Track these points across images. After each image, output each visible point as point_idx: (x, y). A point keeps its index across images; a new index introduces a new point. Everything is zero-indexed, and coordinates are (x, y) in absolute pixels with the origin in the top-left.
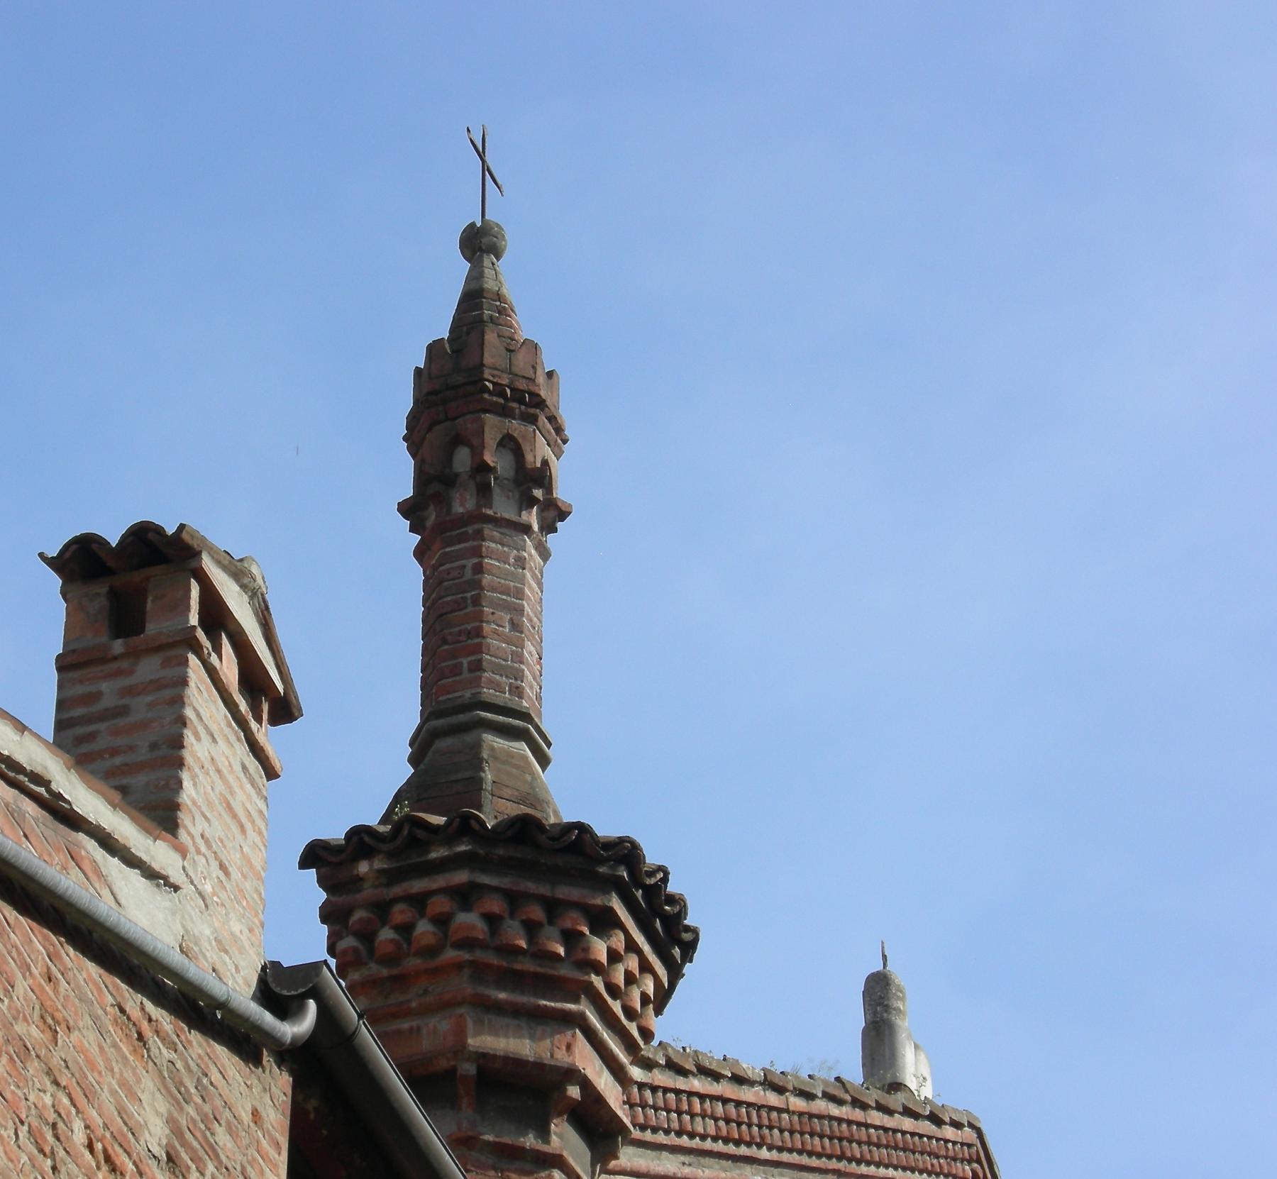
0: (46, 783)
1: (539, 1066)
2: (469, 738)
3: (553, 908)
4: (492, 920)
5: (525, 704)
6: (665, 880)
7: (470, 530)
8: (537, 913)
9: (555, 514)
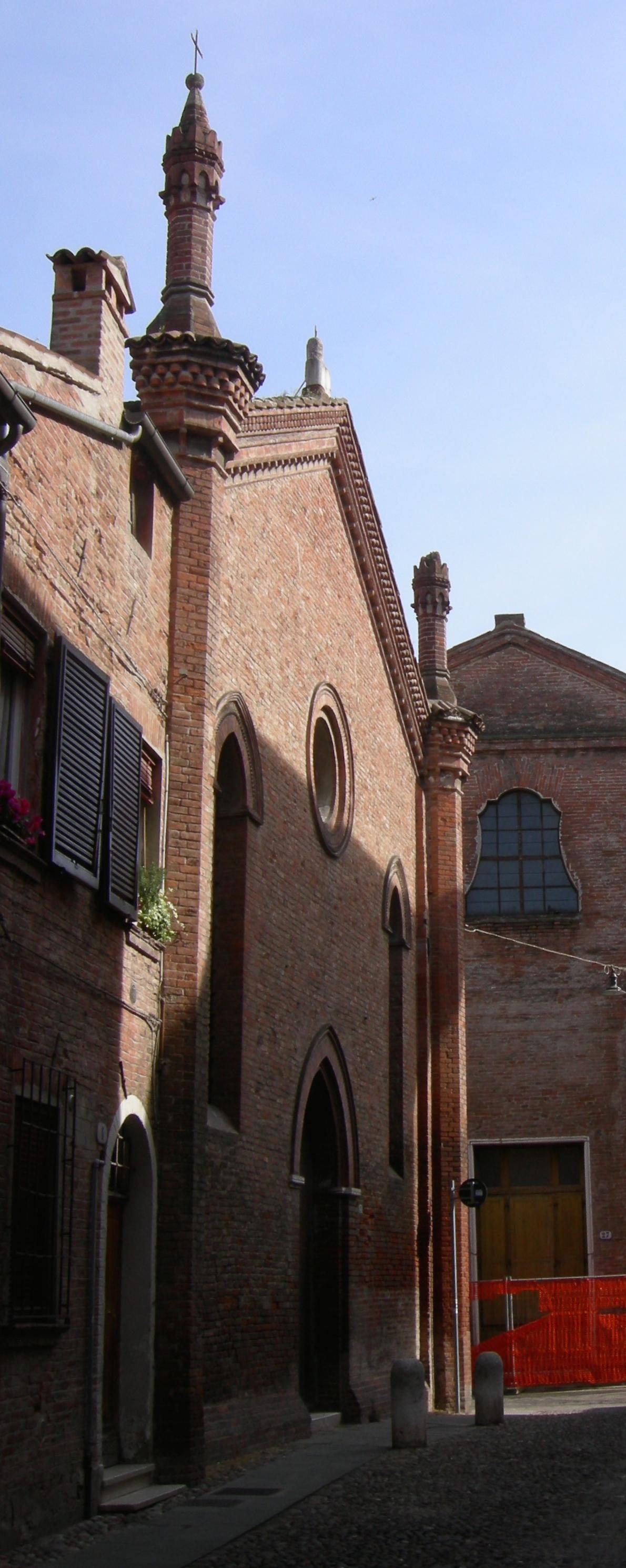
1: (209, 430)
2: (185, 296)
3: (216, 370)
4: (195, 375)
5: (206, 283)
6: (256, 360)
7: (187, 209)
8: (211, 373)
9: (219, 202)
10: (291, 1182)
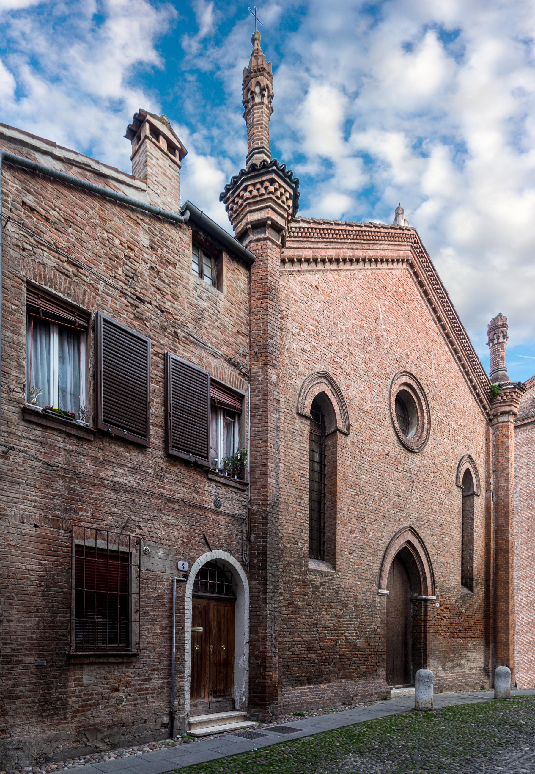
0: (90, 166)
10: (378, 593)
